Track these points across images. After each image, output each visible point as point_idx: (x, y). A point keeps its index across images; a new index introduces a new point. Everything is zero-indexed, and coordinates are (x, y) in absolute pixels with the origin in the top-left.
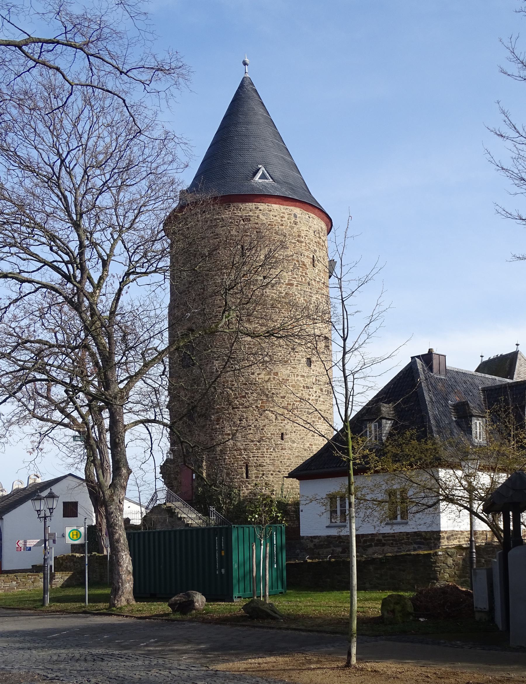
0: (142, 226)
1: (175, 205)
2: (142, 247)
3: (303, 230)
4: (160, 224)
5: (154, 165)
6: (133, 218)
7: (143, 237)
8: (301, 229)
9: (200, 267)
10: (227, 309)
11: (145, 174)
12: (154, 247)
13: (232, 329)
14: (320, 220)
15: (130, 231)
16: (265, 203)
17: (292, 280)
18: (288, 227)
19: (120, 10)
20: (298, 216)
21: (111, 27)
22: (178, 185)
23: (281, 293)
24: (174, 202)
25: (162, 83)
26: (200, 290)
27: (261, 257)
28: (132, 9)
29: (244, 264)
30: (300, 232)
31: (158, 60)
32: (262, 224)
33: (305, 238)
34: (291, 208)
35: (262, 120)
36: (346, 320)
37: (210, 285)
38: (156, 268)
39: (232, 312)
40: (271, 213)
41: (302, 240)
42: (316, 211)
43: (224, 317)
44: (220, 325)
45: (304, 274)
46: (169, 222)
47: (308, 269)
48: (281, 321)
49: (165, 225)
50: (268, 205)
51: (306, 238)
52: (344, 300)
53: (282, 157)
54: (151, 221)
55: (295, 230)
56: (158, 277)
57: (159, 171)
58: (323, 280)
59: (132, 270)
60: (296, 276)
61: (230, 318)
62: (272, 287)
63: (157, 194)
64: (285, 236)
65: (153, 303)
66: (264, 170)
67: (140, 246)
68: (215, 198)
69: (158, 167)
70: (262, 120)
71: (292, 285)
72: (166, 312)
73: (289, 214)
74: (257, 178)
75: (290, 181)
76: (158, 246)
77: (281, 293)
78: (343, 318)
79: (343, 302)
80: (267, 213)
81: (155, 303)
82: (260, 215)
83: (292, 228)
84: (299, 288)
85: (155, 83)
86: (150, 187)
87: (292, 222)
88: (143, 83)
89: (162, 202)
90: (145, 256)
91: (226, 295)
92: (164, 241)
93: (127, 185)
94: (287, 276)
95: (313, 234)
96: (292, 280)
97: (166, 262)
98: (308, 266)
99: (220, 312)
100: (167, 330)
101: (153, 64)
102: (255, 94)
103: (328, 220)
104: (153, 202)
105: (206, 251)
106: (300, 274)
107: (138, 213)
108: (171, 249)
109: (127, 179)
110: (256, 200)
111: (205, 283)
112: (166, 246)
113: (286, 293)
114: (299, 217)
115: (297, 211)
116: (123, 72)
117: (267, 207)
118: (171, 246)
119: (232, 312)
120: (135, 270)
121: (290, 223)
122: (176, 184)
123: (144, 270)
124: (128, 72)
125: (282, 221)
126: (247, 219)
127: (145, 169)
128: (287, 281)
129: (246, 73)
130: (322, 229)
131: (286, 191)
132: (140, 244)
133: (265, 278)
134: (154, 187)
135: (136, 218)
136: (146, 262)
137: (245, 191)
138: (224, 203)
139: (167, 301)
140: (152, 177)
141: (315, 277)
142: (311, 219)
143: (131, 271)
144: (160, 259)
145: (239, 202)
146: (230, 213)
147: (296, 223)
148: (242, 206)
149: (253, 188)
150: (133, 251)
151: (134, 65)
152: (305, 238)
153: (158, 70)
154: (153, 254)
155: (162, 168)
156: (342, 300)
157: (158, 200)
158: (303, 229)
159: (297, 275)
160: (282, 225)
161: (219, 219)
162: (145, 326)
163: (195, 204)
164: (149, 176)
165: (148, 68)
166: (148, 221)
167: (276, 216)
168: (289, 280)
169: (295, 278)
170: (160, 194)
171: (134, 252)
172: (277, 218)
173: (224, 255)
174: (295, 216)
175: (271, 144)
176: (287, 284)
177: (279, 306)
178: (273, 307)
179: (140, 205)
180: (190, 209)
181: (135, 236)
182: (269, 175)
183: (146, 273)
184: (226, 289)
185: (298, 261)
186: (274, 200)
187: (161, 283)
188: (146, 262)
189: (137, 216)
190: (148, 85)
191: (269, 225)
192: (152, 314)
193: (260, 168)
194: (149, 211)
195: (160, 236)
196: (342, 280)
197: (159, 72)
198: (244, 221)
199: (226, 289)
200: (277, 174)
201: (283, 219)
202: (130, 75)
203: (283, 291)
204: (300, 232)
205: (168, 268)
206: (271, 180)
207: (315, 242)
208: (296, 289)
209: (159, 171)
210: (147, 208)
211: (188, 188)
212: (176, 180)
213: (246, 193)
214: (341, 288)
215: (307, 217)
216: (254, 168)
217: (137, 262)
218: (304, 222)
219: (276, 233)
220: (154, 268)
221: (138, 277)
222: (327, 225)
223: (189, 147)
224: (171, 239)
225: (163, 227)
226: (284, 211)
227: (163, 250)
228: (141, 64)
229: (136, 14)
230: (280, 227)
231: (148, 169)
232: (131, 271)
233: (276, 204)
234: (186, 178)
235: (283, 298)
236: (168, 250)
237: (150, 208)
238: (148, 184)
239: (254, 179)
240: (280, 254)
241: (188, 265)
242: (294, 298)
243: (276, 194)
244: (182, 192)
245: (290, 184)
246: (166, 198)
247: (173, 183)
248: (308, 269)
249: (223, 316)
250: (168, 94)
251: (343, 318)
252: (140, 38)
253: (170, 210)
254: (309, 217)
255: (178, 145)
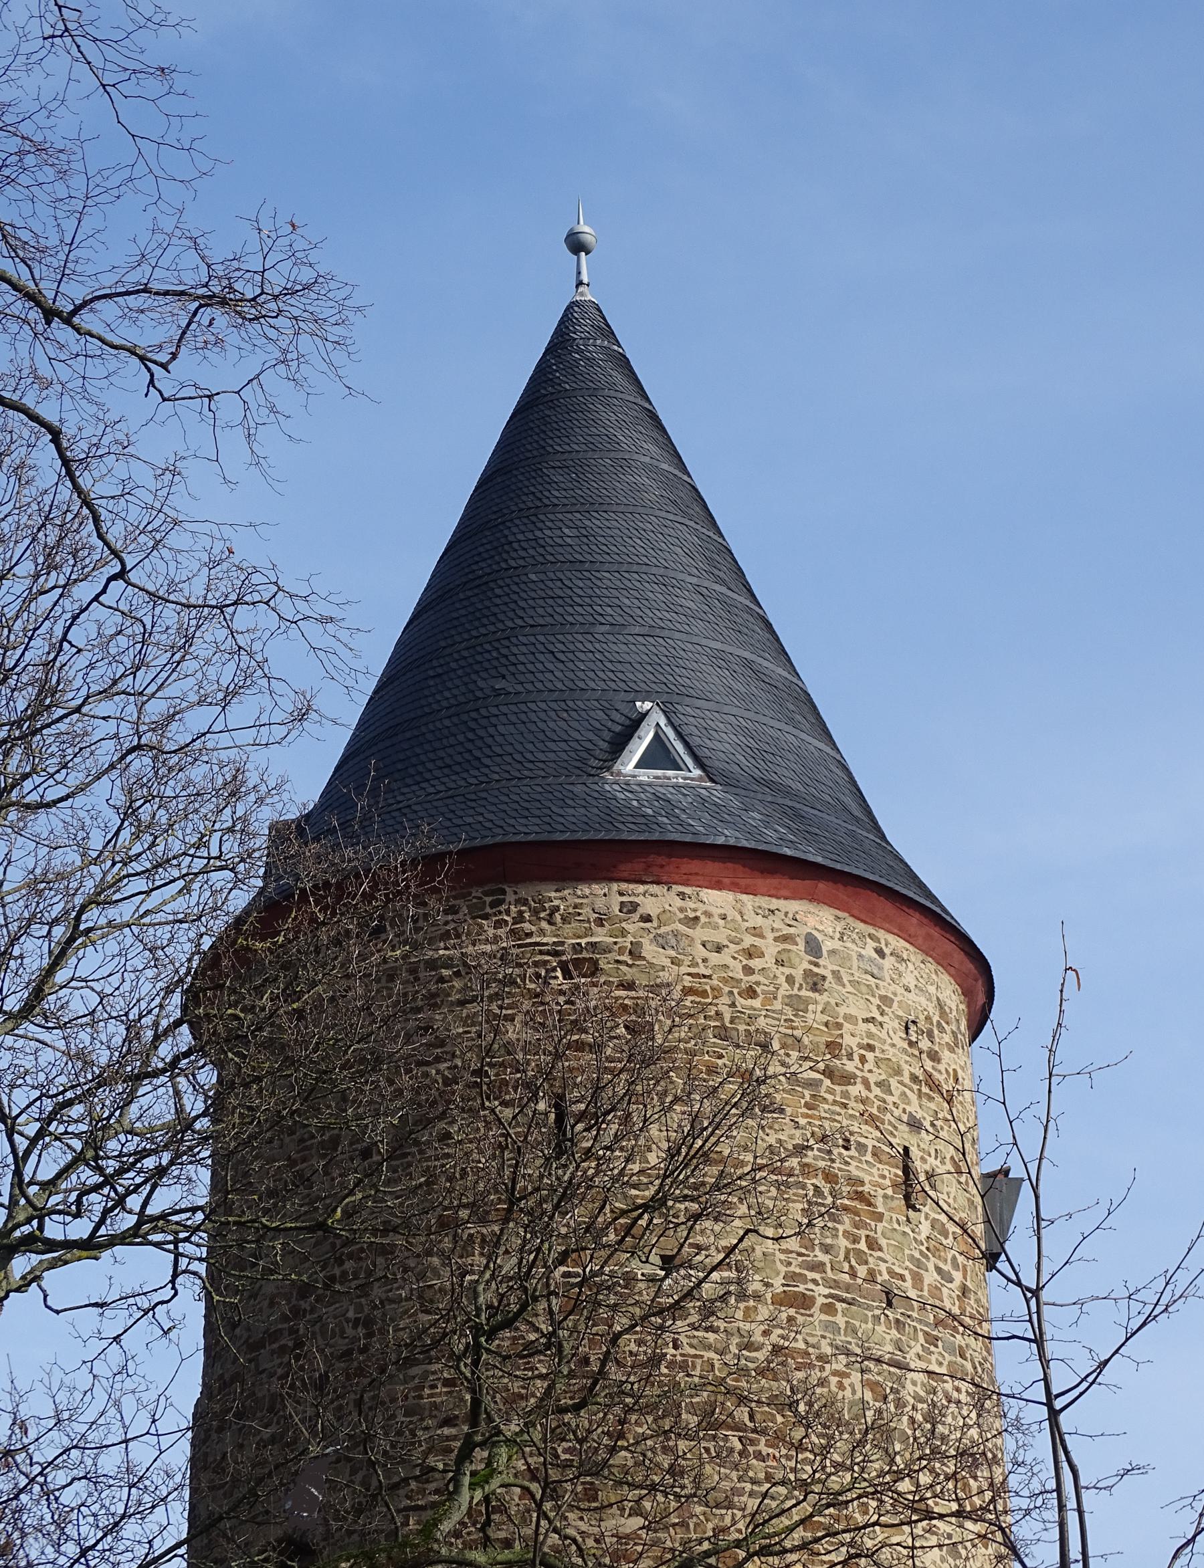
0: (79, 1003)
1: (239, 900)
2: (77, 1110)
3: (849, 1018)
4: (169, 991)
5: (156, 709)
6: (46, 962)
7: (83, 1057)
8: (842, 1010)
9: (347, 1214)
10: (477, 1429)
11: (107, 752)
12: (134, 1110)
13: (507, 1544)
14: (932, 966)
15: (28, 1028)
16: (669, 884)
17: (804, 1279)
18: (777, 1005)
19: (60, 61)
20: (827, 945)
21: (26, 128)
22: (260, 801)
23: (749, 1346)
24: (238, 882)
25: (226, 360)
26: (350, 1332)
27: (653, 1158)
28: (110, 53)
29: (566, 1196)
30: (839, 1026)
31: (216, 256)
32: (655, 988)
33: (863, 1059)
34: (793, 906)
35: (653, 492)
36: (1072, 1519)
37: (399, 1300)
38: (142, 1218)
39: (503, 1451)
40: (699, 934)
41: (850, 1067)
42: (914, 921)
43: (466, 1480)
44: (446, 1526)
45: (863, 1246)
46: (218, 984)
47: (879, 1217)
48: (753, 1504)
49: (193, 997)
50: (682, 896)
51: (870, 1056)
52: (1058, 1404)
53: (748, 664)
54: (125, 976)
55: (815, 1017)
56: (145, 1266)
57: (178, 734)
58: (958, 1276)
59: (26, 1229)
60: (825, 1258)
61: (495, 1483)
62: (708, 1311)
63: (160, 849)
64: (765, 1046)
65: (117, 1404)
66: (663, 722)
67: (69, 1103)
68: (432, 862)
69: (171, 718)
70: (653, 492)
71: (804, 1302)
72: (180, 1455)
73: (785, 938)
74: (629, 763)
75: (787, 776)
76: (154, 1104)
77: (749, 1346)
78: (1061, 1507)
79: (1054, 1415)
80: (676, 934)
81: (129, 1404)
82: (646, 942)
83: (798, 1005)
84: (840, 1320)
85: (198, 357)
86: (129, 812)
87: (799, 979)
88: (142, 359)
89: (181, 883)
90: (91, 1151)
91: (476, 1363)
92: (181, 1080)
93: (28, 806)
94: (775, 1261)
95: (898, 1038)
96: (804, 1279)
97: (190, 1188)
98: (879, 1202)
99: (449, 1450)
100: (182, 1550)
101: (192, 275)
102: (618, 377)
103: (970, 966)
104: (140, 884)
105: (379, 1132)
106: (843, 1243)
107: (72, 939)
108: (215, 1122)
109: (25, 776)
110: (625, 869)
111: (377, 1292)
112: (194, 1104)
113: (777, 1350)
114: (833, 952)
115: (820, 920)
116: (59, 314)
117: (678, 902)
118: (217, 1107)
119: (503, 1451)
120: (41, 1227)
121: (790, 980)
122: (252, 797)
123: (80, 1229)
124: (77, 310)
125: (748, 970)
126: (584, 964)
127: (111, 727)
128: (778, 1282)
129: (580, 283)
130: (943, 1014)
131: (767, 825)
132: (69, 1095)
133: (668, 1263)
134: (145, 813)
135: (57, 962)
136: (96, 1188)
137: (572, 823)
138: (480, 883)
139: (188, 1389)
140: (140, 764)
141: (918, 1263)
142: (889, 962)
143: (17, 1234)
144: (161, 1171)
145: (544, 879)
146: (501, 932)
147: (816, 983)
148: (559, 898)
149: (611, 810)
150: (32, 1129)
151: (107, 282)
152: (863, 1059)
153: (209, 300)
154: (133, 1144)
155: (198, 719)
156: (1049, 1404)
157: (162, 875)
158: (852, 1011)
159: (827, 1249)
160: (751, 993)
161: (447, 963)
162: (70, 1530)
163: (334, 892)
164: (129, 758)
165: (166, 293)
166: (115, 980)
167: (719, 949)
168: (792, 1277)
169: (818, 1267)
170: (177, 847)
171: (40, 1134)
172: (725, 958)
173: (471, 1148)
174: (813, 947)
175: (691, 603)
176: (779, 1301)
177: (742, 1414)
178: (710, 1422)
179: (78, 900)
180: (313, 919)
181: (47, 1056)
182: (687, 745)
183: (90, 1246)
184: (477, 1330)
185: (830, 1177)
186: (712, 867)
187: (156, 1297)
188: (96, 1188)
189: (63, 953)
190: (164, 366)
191: (688, 991)
192: (110, 1462)
193: (644, 716)
194: (121, 927)
195: (165, 1050)
196: (1045, 1295)
197: (216, 312)
198: (567, 975)
199: (477, 1330)
200: (724, 745)
201: (756, 963)
202: (86, 326)
203: (758, 1338)
204: (839, 1026)
205: (200, 1216)
206: (697, 772)
207: (914, 1078)
208: (827, 1326)
209: (178, 734)
210: (112, 913)
211: (307, 817)
212: (253, 779)
213: (580, 836)
214: (1039, 1341)
215: (869, 951)
216: (617, 717)
217: (49, 1186)
218: (858, 975)
219: (723, 1033)
220: (131, 1220)
221: (53, 1265)
222: (967, 993)
223: (344, 635)
224: (219, 1065)
225: (184, 1008)
226: (759, 921)
227: (184, 1123)
228: (135, 278)
229: (126, 75)
230: (740, 1001)
231: (125, 729)
232: (17, 1234)
233: (718, 886)
234: (300, 772)
235: (761, 1372)
236: (203, 1124)
237: (125, 912)
238: (120, 799)
239: (617, 766)
240: (743, 1143)
241: (293, 1204)
242: (816, 1374)
243: (721, 840)
244: (279, 832)
245: (787, 792)
246: (199, 864)
247: (233, 791)
248: (879, 1217)
249: (458, 1472)
250: (253, 405)
251: (1061, 1507)
252: (140, 169)
253: (219, 925)
254: (880, 953)
255: (294, 632)
